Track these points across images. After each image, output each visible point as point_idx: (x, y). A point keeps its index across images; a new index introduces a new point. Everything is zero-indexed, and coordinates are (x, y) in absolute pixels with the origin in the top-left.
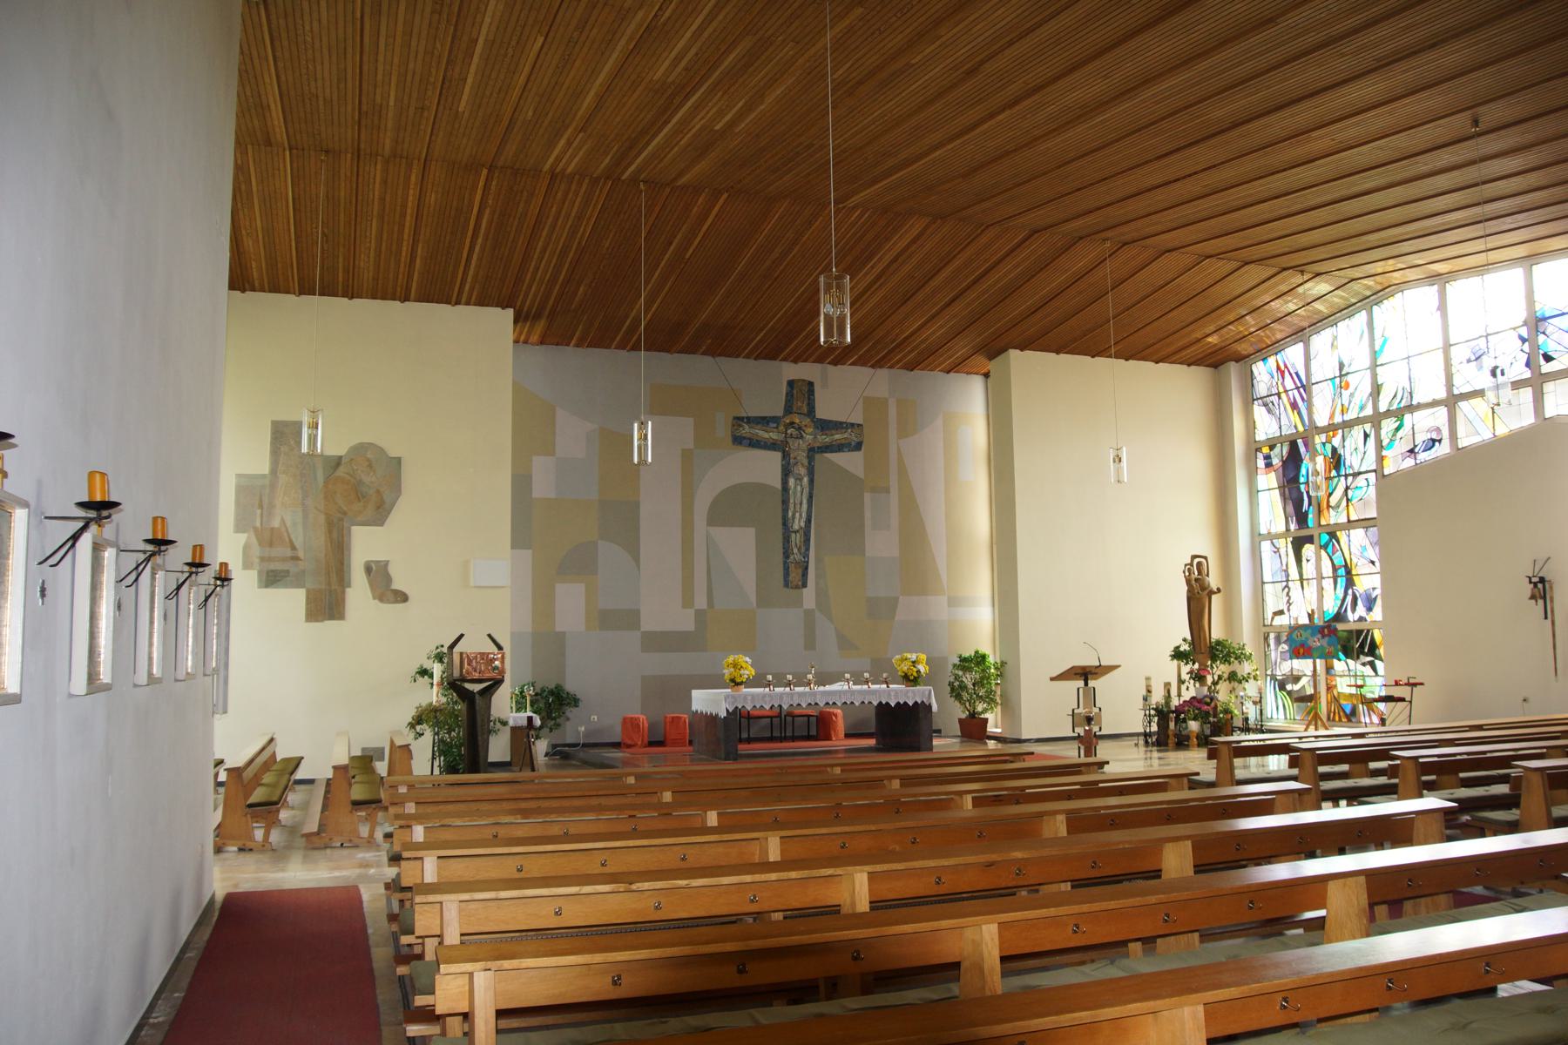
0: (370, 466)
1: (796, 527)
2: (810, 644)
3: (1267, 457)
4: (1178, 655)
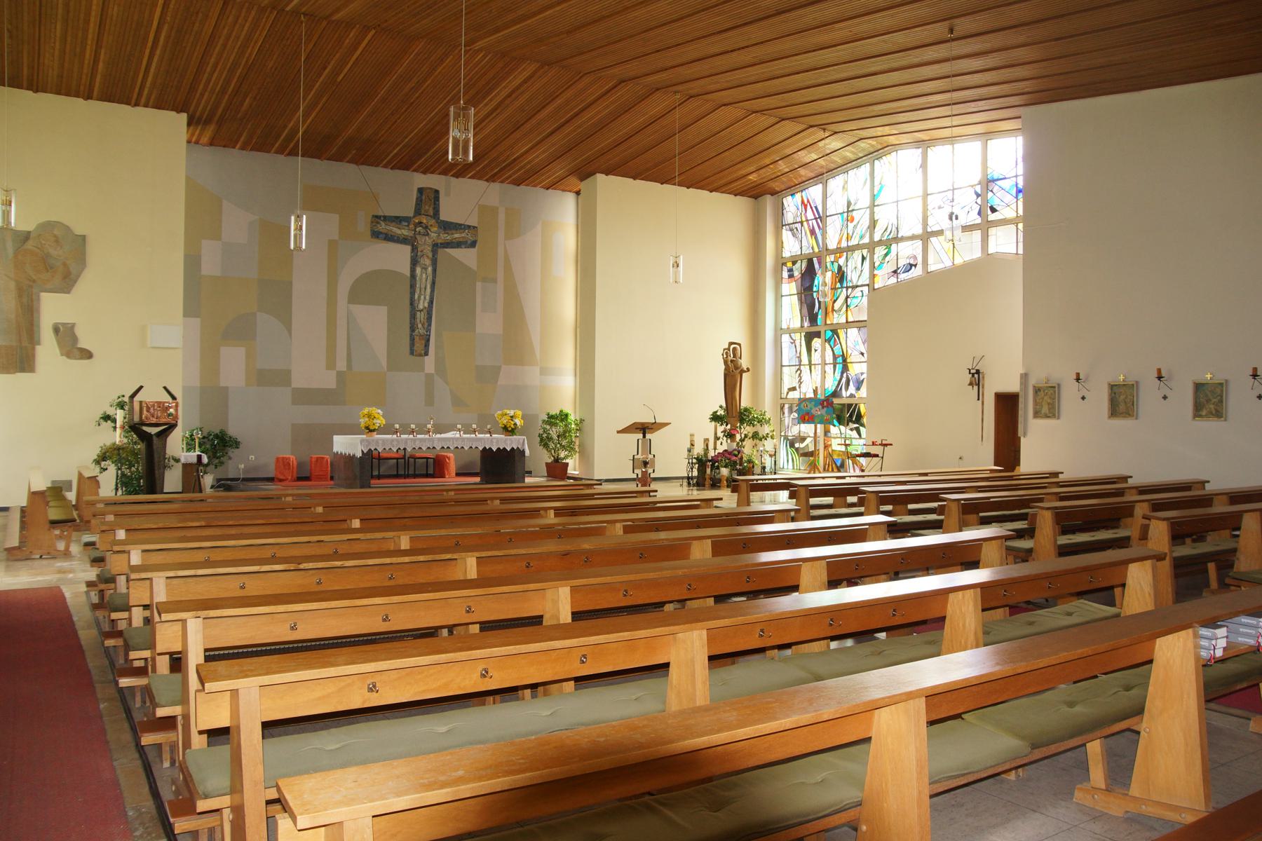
0: (57, 241)
1: (421, 307)
2: (430, 400)
3: (790, 270)
4: (715, 418)
